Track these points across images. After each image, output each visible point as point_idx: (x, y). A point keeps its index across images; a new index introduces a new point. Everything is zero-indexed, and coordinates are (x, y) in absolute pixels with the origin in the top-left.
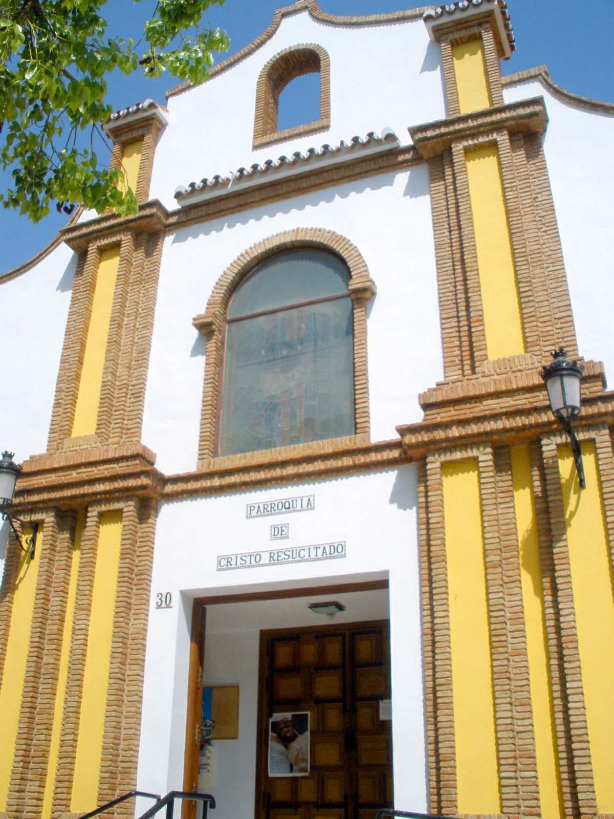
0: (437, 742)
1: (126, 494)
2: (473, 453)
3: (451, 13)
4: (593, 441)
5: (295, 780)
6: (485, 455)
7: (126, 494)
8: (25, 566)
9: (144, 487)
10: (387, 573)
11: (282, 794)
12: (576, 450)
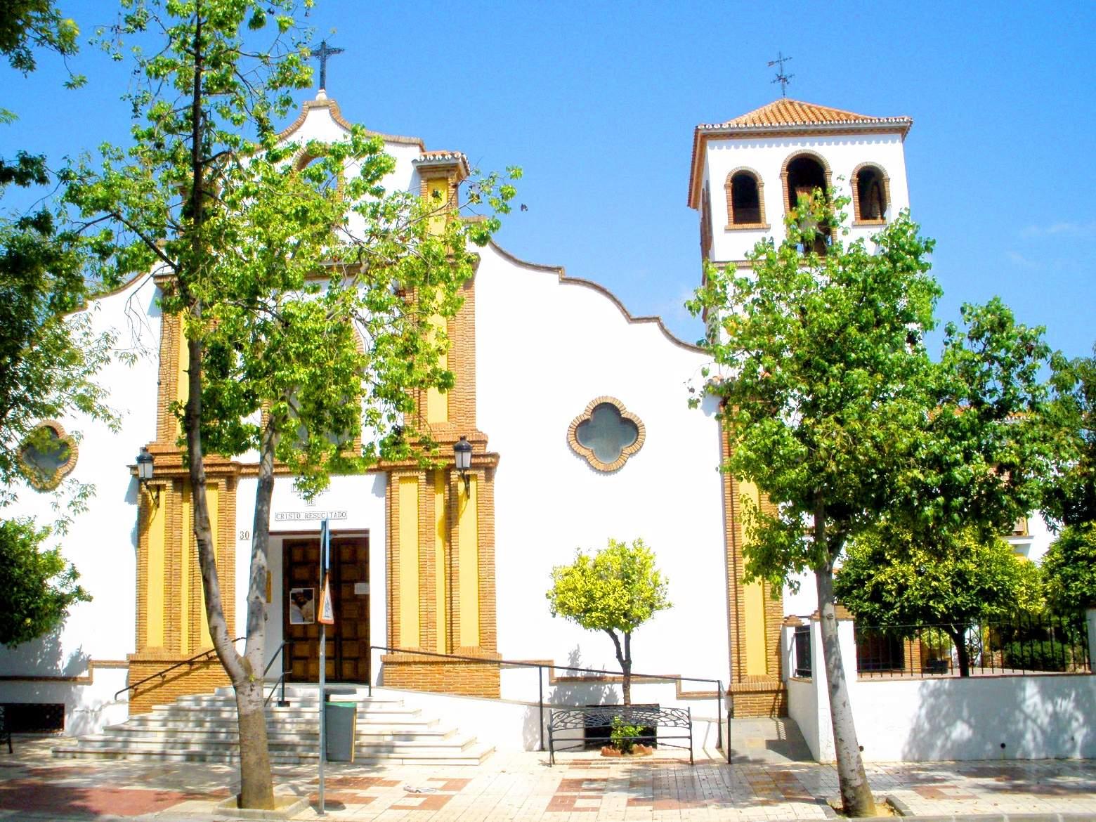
0: (392, 615)
1: (220, 475)
2: (416, 474)
3: (430, 161)
4: (476, 475)
5: (305, 626)
6: (422, 476)
7: (220, 475)
8: (154, 511)
9: (231, 472)
10: (366, 532)
11: (298, 633)
12: (467, 479)
